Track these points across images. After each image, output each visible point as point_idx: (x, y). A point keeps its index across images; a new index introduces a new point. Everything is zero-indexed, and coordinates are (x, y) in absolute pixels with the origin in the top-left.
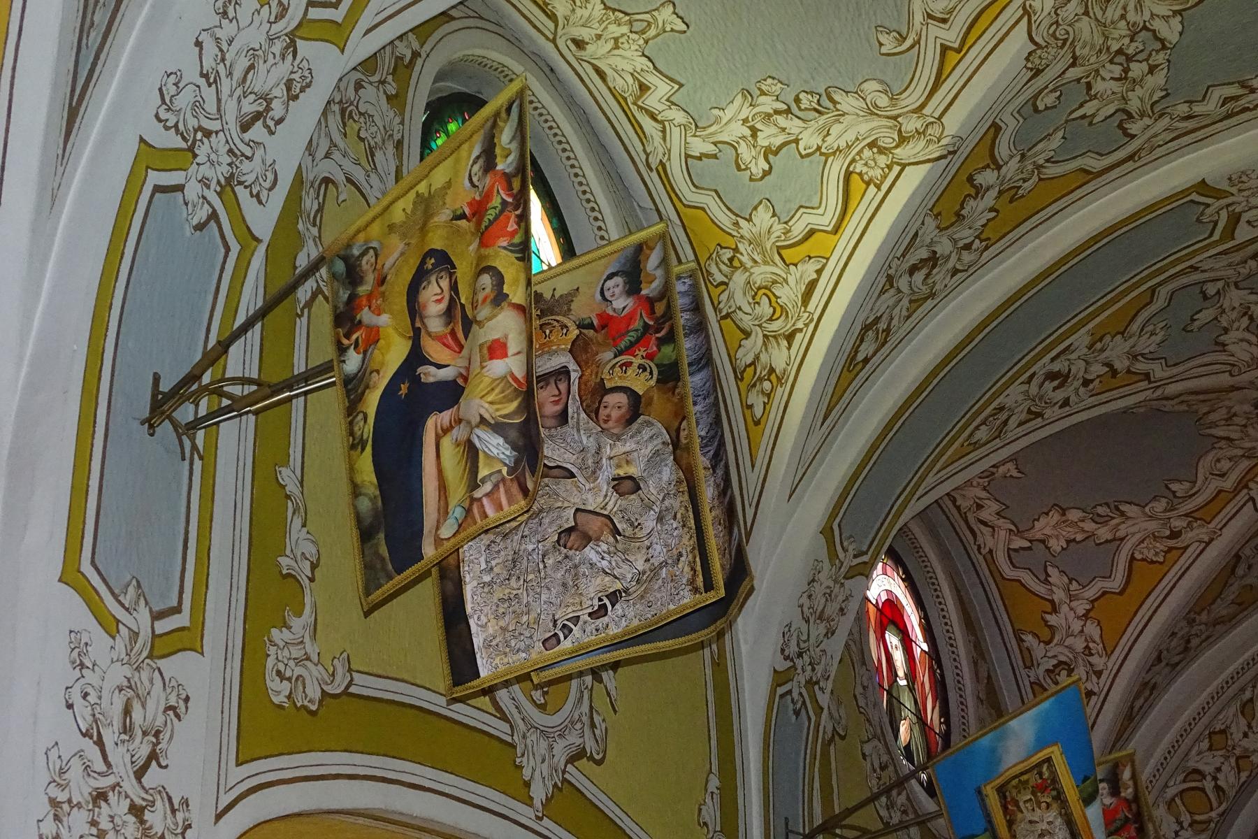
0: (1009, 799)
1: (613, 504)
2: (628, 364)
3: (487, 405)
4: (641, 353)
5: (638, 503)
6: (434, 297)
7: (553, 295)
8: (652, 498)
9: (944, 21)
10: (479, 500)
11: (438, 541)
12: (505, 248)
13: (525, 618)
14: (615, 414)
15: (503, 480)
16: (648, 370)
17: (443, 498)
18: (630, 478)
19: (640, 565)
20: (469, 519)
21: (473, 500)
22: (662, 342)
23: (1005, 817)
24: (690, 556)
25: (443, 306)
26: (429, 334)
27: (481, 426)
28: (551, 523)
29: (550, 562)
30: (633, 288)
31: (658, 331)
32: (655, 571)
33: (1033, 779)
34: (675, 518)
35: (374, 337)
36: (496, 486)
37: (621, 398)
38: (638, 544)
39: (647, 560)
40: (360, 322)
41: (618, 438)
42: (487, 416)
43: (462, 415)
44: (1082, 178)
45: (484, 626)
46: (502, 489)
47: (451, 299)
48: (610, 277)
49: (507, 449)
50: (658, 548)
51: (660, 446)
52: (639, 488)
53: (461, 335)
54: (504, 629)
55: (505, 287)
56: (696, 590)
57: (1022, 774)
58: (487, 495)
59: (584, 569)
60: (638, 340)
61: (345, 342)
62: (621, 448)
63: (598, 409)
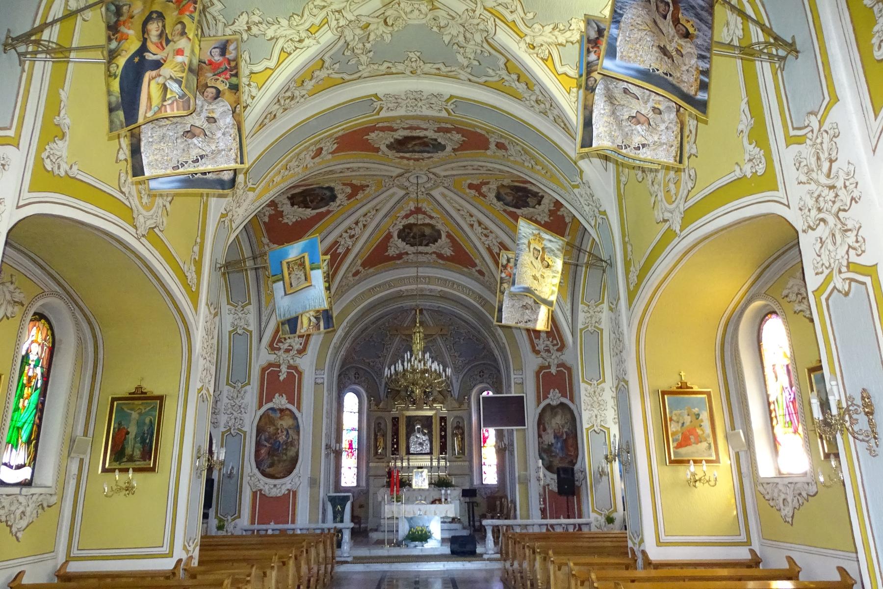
1: (206, 125)
2: (218, 79)
5: (215, 127)
6: (154, 28)
9: (315, 16)
10: (165, 106)
13: (166, 158)
14: (211, 95)
15: (176, 100)
18: (213, 118)
21: (163, 105)
22: (232, 75)
26: (152, 42)
28: (181, 128)
29: (179, 141)
32: (219, 152)
33: (299, 262)
35: (126, 38)
36: (172, 103)
37: (214, 91)
41: (210, 103)
43: (161, 73)
44: (342, 81)
45: (148, 157)
46: (175, 104)
48: (215, 48)
53: (164, 44)
54: (157, 160)
59: (191, 146)
62: (211, 107)
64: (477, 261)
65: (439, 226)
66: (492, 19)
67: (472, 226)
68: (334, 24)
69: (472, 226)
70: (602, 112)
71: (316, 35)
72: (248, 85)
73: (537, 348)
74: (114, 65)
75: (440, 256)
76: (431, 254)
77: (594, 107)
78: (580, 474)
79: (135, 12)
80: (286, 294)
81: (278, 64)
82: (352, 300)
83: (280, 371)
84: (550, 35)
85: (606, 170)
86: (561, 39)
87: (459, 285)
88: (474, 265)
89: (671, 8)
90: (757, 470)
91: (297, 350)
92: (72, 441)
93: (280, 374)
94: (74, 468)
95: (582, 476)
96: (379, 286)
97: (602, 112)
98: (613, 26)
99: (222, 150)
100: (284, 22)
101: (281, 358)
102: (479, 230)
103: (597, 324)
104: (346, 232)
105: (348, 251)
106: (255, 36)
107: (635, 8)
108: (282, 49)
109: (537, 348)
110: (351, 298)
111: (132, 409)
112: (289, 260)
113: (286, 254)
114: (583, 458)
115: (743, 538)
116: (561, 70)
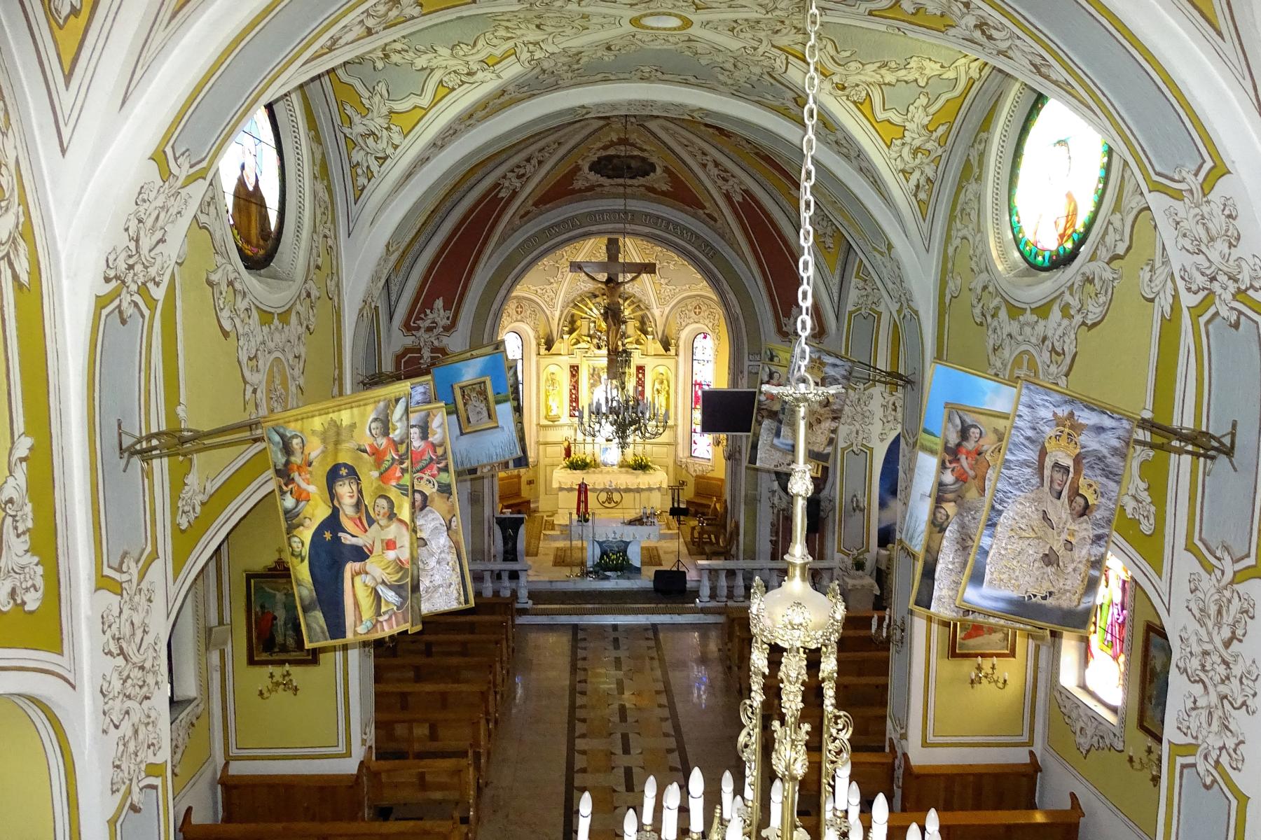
2: (421, 478)
6: (345, 491)
10: (381, 622)
11: (355, 633)
15: (395, 613)
19: (428, 584)
21: (377, 621)
22: (440, 470)
25: (354, 500)
26: (346, 515)
30: (424, 436)
32: (436, 588)
33: (477, 387)
36: (390, 617)
40: (293, 479)
43: (368, 569)
50: (437, 577)
52: (426, 544)
56: (460, 603)
60: (427, 465)
61: (284, 488)
64: (707, 205)
65: (654, 160)
66: (784, 57)
67: (704, 166)
68: (525, 56)
69: (704, 166)
70: (950, 567)
71: (496, 67)
72: (386, 129)
73: (784, 329)
74: (296, 539)
75: (651, 189)
76: (639, 186)
77: (941, 555)
78: (827, 503)
79: (313, 455)
80: (462, 434)
81: (434, 104)
82: (517, 248)
83: (421, 357)
84: (873, 74)
85: (928, 251)
86: (890, 77)
87: (676, 225)
88: (703, 208)
89: (1071, 475)
90: (1058, 674)
91: (443, 327)
92: (209, 631)
94: (215, 657)
95: (830, 507)
96: (557, 225)
97: (950, 567)
98: (986, 532)
99: (439, 586)
100: (444, 52)
102: (715, 171)
103: (874, 306)
104: (512, 171)
105: (514, 194)
106: (396, 64)
107: (1021, 504)
108: (441, 82)
109: (784, 329)
110: (516, 244)
112: (464, 384)
113: (458, 374)
114: (834, 484)
115: (1025, 738)
116: (881, 115)
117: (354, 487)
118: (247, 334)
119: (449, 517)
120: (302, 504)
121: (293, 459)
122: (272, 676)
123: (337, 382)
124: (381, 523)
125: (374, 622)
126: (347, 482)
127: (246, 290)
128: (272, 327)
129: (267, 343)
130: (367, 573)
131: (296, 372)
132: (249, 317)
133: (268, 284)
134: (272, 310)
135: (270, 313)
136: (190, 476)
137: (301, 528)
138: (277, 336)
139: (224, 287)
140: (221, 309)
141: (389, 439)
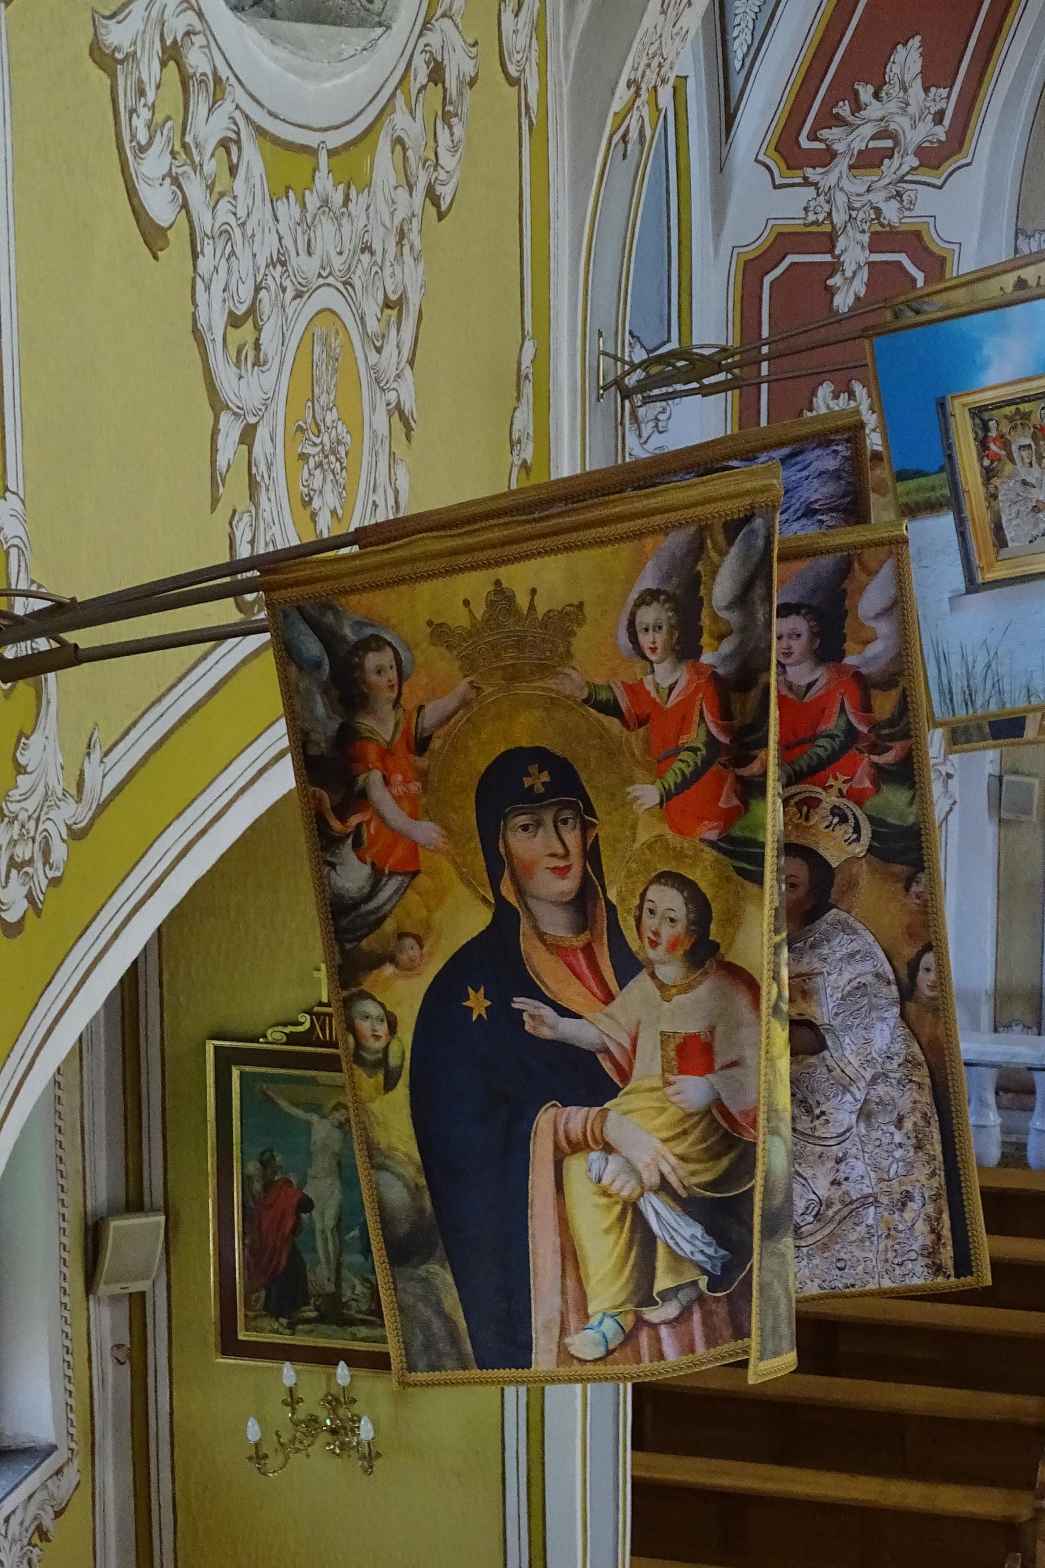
0: (993, 434)
3: (674, 1160)
4: (838, 784)
7: (532, 607)
8: (849, 1070)
10: (654, 1326)
12: (712, 844)
15: (701, 1299)
16: (852, 820)
17: (571, 1283)
19: (822, 1188)
20: (628, 1350)
21: (640, 1322)
22: (882, 775)
23: (981, 459)
24: (930, 1209)
25: (568, 885)
26: (541, 936)
27: (662, 1194)
31: (876, 749)
32: (854, 1207)
34: (899, 1123)
36: (684, 1316)
38: (819, 1149)
39: (835, 1183)
42: (672, 1179)
43: (612, 1134)
46: (697, 1317)
47: (585, 878)
49: (709, 1245)
50: (860, 1168)
51: (869, 979)
52: (823, 1046)
55: (713, 927)
56: (938, 1269)
57: (1024, 400)
58: (668, 1323)
60: (833, 758)
61: (336, 824)
63: (640, 907)
74: (371, 1008)
80: (972, 586)
83: (835, 267)
91: (919, 151)
93: (836, 281)
101: (840, 199)
111: (314, 1107)
117: (572, 838)
118: (226, 233)
119: (909, 951)
120: (391, 886)
121: (366, 722)
122: (292, 1399)
123: (528, 389)
124: (663, 973)
125: (629, 1321)
126: (548, 817)
127: (224, 72)
128: (312, 201)
129: (294, 261)
130: (608, 1149)
131: (390, 358)
132: (233, 170)
133: (298, 46)
134: (311, 139)
135: (305, 149)
136: (36, 741)
137: (389, 969)
138: (326, 232)
139: (150, 69)
140: (143, 149)
141: (698, 670)
